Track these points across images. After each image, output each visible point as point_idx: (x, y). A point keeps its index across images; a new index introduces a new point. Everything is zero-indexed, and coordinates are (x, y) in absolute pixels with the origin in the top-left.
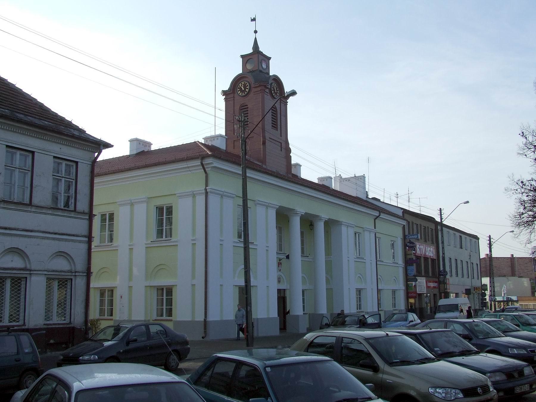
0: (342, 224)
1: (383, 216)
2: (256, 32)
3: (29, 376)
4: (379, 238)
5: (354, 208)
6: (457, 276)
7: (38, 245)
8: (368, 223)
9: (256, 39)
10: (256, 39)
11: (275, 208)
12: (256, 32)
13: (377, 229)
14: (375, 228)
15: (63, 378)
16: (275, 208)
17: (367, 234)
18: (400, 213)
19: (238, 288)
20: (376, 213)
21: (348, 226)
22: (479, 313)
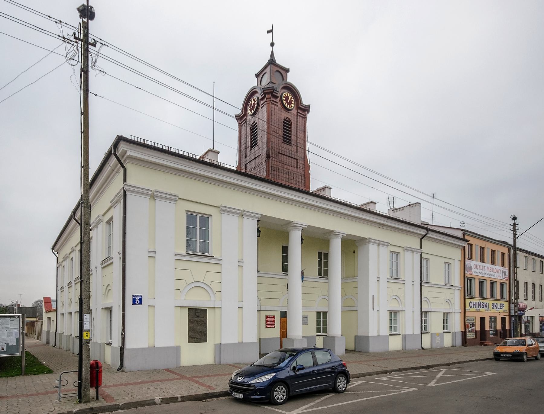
0: (369, 242)
1: (430, 234)
2: (272, 44)
3: (282, 401)
4: (427, 259)
5: (387, 224)
6: (534, 300)
7: (96, 268)
8: (414, 243)
9: (272, 52)
10: (272, 52)
11: (256, 217)
12: (272, 44)
13: (424, 250)
14: (421, 247)
15: (257, 406)
16: (256, 217)
17: (408, 255)
18: (460, 234)
19: (186, 312)
20: (423, 232)
21: (379, 245)
22: (521, 342)
